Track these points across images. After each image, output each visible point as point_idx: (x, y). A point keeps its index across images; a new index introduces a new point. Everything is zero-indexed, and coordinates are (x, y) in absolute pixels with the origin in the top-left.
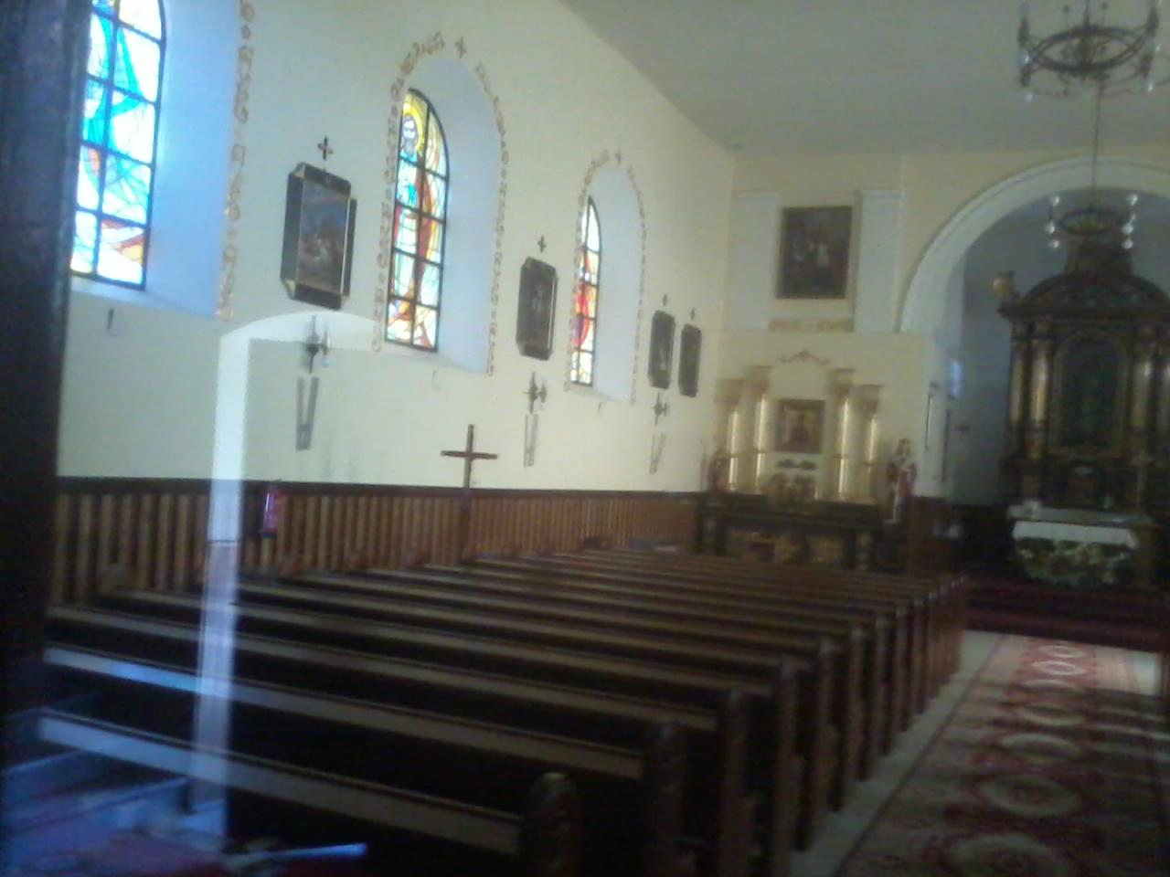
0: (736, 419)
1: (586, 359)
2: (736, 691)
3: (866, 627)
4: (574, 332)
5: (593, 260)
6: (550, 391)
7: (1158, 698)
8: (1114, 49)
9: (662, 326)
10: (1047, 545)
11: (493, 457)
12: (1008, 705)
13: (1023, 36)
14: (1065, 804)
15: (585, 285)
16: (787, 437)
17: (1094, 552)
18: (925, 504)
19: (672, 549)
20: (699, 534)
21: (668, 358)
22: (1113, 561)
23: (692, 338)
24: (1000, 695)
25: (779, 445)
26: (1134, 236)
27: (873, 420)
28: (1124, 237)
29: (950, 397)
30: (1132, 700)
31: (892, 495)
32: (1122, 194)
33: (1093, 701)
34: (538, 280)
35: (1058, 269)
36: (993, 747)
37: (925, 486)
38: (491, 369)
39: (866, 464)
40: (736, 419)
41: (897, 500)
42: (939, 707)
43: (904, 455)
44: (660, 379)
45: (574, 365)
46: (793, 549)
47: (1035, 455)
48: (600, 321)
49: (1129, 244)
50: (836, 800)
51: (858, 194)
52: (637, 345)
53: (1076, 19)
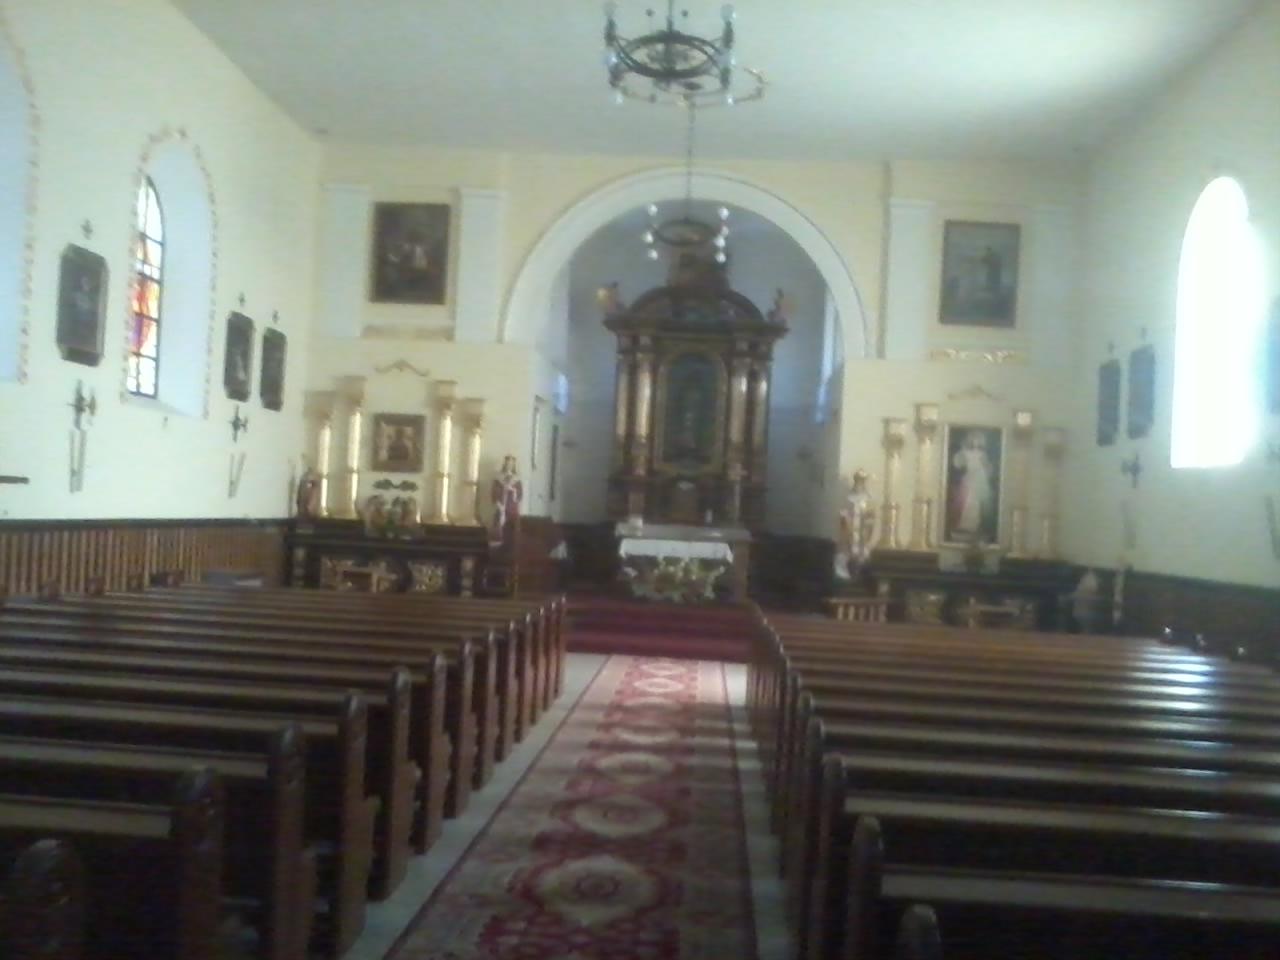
0: (327, 436)
1: (148, 366)
2: (288, 731)
3: (448, 654)
4: (131, 334)
5: (154, 252)
6: (99, 401)
7: (746, 708)
8: (698, 57)
9: (239, 330)
10: (651, 561)
11: (24, 480)
12: (607, 727)
13: (611, 37)
14: (656, 819)
15: (144, 279)
16: (384, 454)
17: (695, 568)
18: (532, 525)
19: (256, 583)
20: (288, 562)
21: (246, 367)
22: (713, 575)
23: (275, 344)
24: (600, 717)
25: (376, 465)
26: (727, 251)
27: (477, 437)
28: (716, 249)
29: (556, 412)
30: (726, 712)
31: (497, 515)
32: (713, 206)
33: (689, 715)
34: (82, 276)
35: (660, 280)
36: (590, 770)
37: (531, 504)
38: (22, 376)
39: (470, 484)
40: (327, 436)
41: (503, 519)
42: (535, 736)
43: (510, 473)
44: (236, 389)
45: (133, 372)
46: (393, 577)
47: (641, 471)
48: (164, 324)
49: (721, 258)
50: (419, 841)
51: (456, 192)
52: (210, 351)
53: (659, 24)
